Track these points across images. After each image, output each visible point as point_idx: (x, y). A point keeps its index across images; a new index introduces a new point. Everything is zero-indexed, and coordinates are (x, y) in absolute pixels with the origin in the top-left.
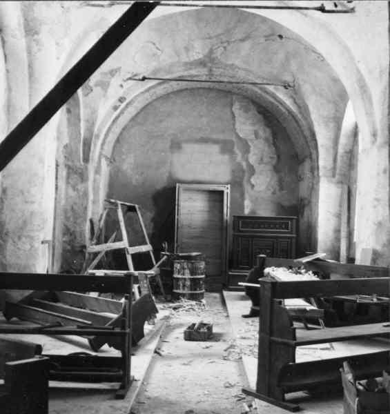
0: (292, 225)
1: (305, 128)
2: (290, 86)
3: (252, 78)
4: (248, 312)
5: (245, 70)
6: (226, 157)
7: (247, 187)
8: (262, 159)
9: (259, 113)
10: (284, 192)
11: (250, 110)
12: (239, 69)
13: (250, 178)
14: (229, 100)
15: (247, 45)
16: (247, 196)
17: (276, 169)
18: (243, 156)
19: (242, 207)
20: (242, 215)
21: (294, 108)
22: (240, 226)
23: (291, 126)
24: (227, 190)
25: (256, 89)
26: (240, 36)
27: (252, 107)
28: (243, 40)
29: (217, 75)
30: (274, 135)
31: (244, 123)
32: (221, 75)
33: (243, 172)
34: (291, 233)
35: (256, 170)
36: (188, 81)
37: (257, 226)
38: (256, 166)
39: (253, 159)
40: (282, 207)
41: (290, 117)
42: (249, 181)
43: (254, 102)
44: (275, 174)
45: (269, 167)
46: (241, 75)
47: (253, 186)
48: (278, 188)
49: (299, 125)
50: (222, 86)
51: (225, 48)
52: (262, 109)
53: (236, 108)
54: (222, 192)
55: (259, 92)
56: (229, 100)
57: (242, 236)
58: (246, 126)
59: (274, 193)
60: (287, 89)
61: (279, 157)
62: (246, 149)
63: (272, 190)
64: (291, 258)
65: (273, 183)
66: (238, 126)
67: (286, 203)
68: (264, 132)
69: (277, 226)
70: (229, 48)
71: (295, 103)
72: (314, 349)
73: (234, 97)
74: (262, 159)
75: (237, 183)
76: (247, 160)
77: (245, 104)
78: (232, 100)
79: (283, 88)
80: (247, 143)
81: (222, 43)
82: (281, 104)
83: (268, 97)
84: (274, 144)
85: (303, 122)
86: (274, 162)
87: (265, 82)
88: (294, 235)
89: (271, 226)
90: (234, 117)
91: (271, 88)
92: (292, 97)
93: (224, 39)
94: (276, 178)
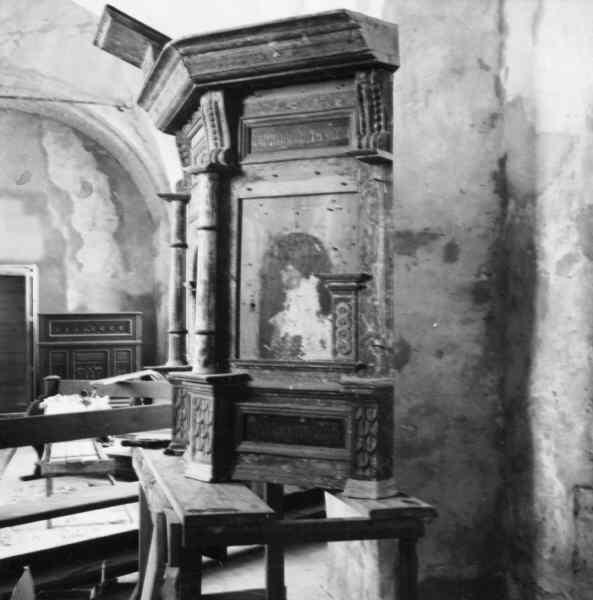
0: (134, 327)
1: (155, 172)
2: (125, 106)
3: (66, 94)
4: (30, 471)
5: (55, 79)
6: (34, 220)
7: (71, 267)
8: (94, 225)
9: (87, 149)
10: (132, 274)
11: (71, 144)
12: (43, 76)
13: (75, 252)
14: (35, 127)
15: (51, 38)
16: (70, 282)
17: (118, 237)
18: (63, 216)
19: (63, 299)
20: (65, 313)
21: (135, 143)
22: (50, 330)
23: (132, 166)
24: (32, 275)
25: (73, 110)
26: (40, 24)
27: (73, 138)
28: (44, 30)
29: (9, 87)
30: (113, 184)
31: (62, 166)
32: (15, 88)
33: (63, 242)
34: (134, 337)
35: (86, 241)
36: (257, 163)
37: (67, 329)
38: (84, 233)
39: (79, 221)
40: (129, 297)
41: (132, 156)
42: (74, 258)
43: (77, 132)
44: (115, 246)
45: (108, 236)
46: (48, 88)
47: (80, 266)
48: (120, 268)
49: (145, 168)
50: (21, 105)
51: (16, 42)
52: (92, 144)
53: (49, 140)
54: (21, 280)
55: (81, 115)
56: (35, 127)
57: (55, 347)
58: (67, 168)
59: (114, 276)
60: (121, 111)
61: (121, 219)
62: (67, 207)
63: (112, 271)
64: (85, 379)
65: (113, 260)
66: (51, 169)
67: (135, 292)
68: (99, 181)
69: (67, 329)
70: (21, 43)
71: (137, 133)
72: (78, 536)
73: (45, 124)
74: (94, 225)
75: (52, 263)
76: (69, 224)
77: (62, 135)
78: (40, 127)
79: (115, 110)
80: (68, 197)
81: (11, 34)
82: (117, 135)
83: (94, 123)
84: (114, 199)
85: (150, 163)
86: (115, 225)
87: (88, 99)
88: (139, 341)
89: (111, 328)
90: (45, 153)
91: (96, 110)
92: (131, 124)
93: (14, 28)
94: (117, 253)
